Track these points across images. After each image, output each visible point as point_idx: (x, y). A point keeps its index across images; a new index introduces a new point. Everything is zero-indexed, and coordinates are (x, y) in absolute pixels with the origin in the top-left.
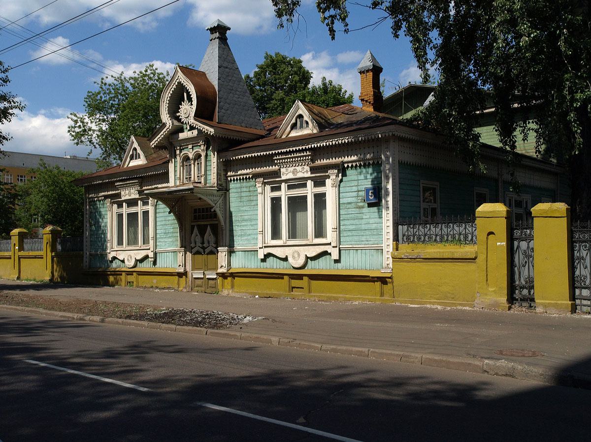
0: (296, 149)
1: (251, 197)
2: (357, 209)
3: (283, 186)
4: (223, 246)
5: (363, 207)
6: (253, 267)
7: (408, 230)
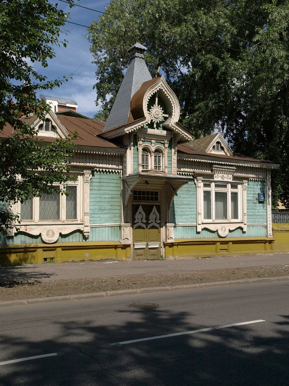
0: (230, 164)
1: (189, 188)
2: (254, 204)
3: (213, 185)
4: (171, 222)
5: (256, 203)
6: (190, 237)
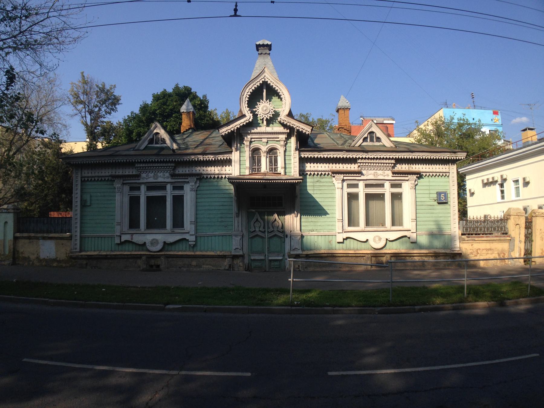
7: (466, 224)
